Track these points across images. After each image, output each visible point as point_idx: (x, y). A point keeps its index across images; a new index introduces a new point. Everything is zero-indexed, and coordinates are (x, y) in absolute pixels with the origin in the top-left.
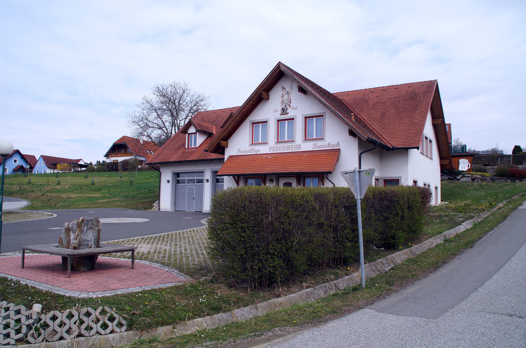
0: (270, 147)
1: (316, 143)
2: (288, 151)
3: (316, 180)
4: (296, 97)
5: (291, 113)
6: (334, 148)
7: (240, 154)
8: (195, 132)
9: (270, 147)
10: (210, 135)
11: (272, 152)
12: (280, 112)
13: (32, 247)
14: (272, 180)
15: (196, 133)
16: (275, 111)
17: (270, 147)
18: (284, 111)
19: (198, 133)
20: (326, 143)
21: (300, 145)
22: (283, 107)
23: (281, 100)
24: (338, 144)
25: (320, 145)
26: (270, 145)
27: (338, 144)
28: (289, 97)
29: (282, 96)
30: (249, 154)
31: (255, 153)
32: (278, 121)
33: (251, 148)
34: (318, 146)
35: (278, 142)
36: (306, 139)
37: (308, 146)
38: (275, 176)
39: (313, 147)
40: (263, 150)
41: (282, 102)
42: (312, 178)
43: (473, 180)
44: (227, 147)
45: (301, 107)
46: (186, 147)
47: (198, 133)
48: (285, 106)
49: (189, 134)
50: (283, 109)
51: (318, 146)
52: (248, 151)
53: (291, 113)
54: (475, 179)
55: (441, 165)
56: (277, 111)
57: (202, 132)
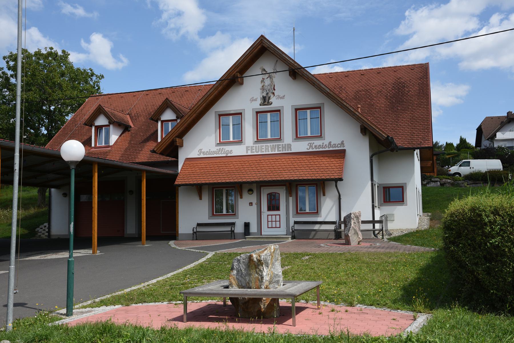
0: (247, 147)
1: (312, 142)
2: (273, 153)
3: (313, 189)
4: (282, 84)
5: (275, 103)
6: (337, 149)
7: (202, 156)
8: (175, 118)
9: (247, 147)
10: (126, 128)
11: (249, 153)
12: (259, 101)
13: (197, 290)
14: (250, 191)
15: (108, 126)
16: (253, 100)
17: (247, 146)
18: (265, 100)
19: (111, 126)
20: (326, 142)
21: (290, 145)
22: (264, 95)
23: (260, 86)
24: (342, 143)
25: (318, 145)
26: (247, 145)
27: (342, 143)
28: (272, 82)
29: (263, 81)
30: (215, 155)
31: (225, 155)
32: (257, 113)
33: (218, 148)
34: (315, 146)
35: (258, 141)
36: (297, 137)
37: (302, 146)
38: (255, 185)
39: (308, 147)
40: (237, 150)
41: (263, 88)
42: (307, 186)
43: (442, 185)
44: (182, 146)
45: (289, 97)
46: (93, 145)
47: (111, 126)
48: (267, 94)
49: (162, 122)
50: (264, 98)
51: (315, 146)
52: (214, 152)
53: (275, 103)
54: (445, 183)
55: (421, 167)
56: (256, 100)
57: (114, 122)
